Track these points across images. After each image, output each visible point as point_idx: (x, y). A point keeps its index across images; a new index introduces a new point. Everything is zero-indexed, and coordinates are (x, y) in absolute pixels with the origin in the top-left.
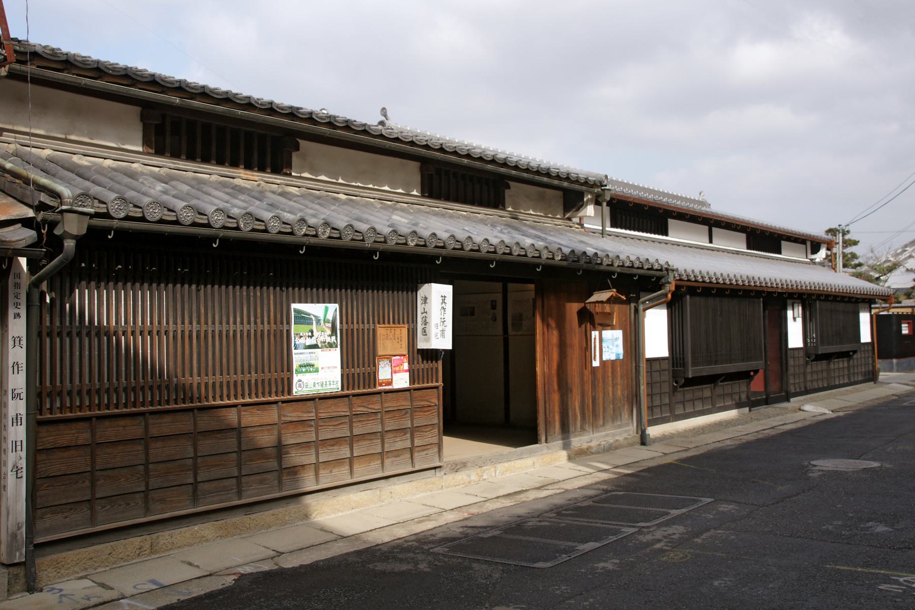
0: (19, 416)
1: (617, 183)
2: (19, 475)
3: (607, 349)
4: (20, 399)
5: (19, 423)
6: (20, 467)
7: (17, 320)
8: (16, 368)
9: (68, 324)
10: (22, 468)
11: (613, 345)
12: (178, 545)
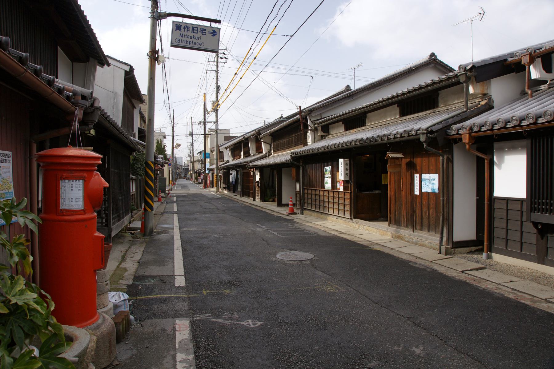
3: (425, 185)
11: (430, 183)
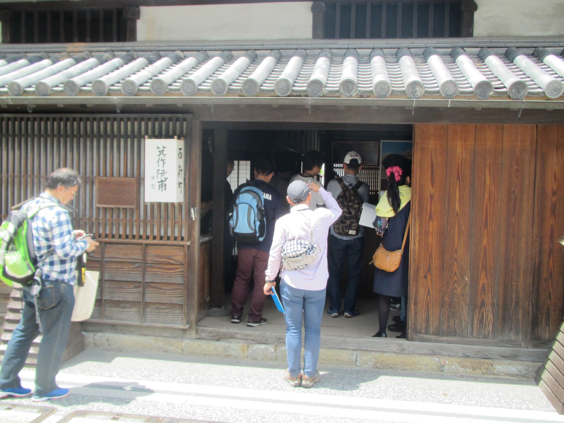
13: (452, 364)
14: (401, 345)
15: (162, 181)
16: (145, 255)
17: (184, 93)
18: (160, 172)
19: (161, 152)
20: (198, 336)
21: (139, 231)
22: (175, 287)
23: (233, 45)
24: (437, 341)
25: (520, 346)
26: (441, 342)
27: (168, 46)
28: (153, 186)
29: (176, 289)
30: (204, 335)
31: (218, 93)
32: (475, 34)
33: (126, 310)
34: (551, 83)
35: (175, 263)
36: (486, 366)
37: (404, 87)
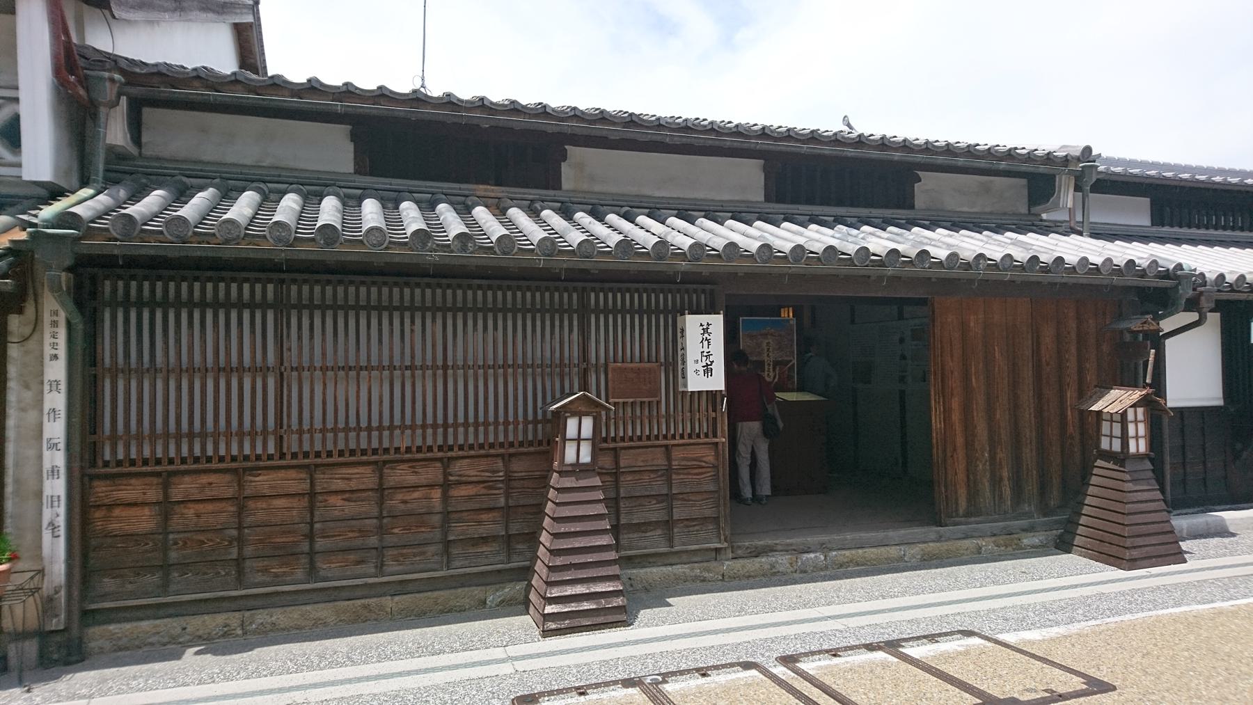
0: (56, 469)
1: (1110, 161)
2: (56, 534)
4: (57, 450)
5: (56, 477)
6: (56, 525)
7: (54, 362)
8: (52, 415)
9: (671, 360)
10: (59, 526)
12: (282, 626)
13: (987, 544)
14: (938, 532)
15: (707, 365)
16: (669, 459)
17: (498, 251)
18: (705, 354)
19: (705, 331)
20: (735, 556)
21: (153, 452)
22: (705, 496)
23: (691, 205)
24: (967, 524)
25: (1032, 517)
26: (970, 523)
27: (613, 200)
28: (697, 371)
29: (707, 499)
30: (740, 552)
31: (797, 261)
32: (916, 207)
33: (648, 534)
34: (544, 239)
35: (707, 465)
36: (1015, 541)
37: (407, 238)
